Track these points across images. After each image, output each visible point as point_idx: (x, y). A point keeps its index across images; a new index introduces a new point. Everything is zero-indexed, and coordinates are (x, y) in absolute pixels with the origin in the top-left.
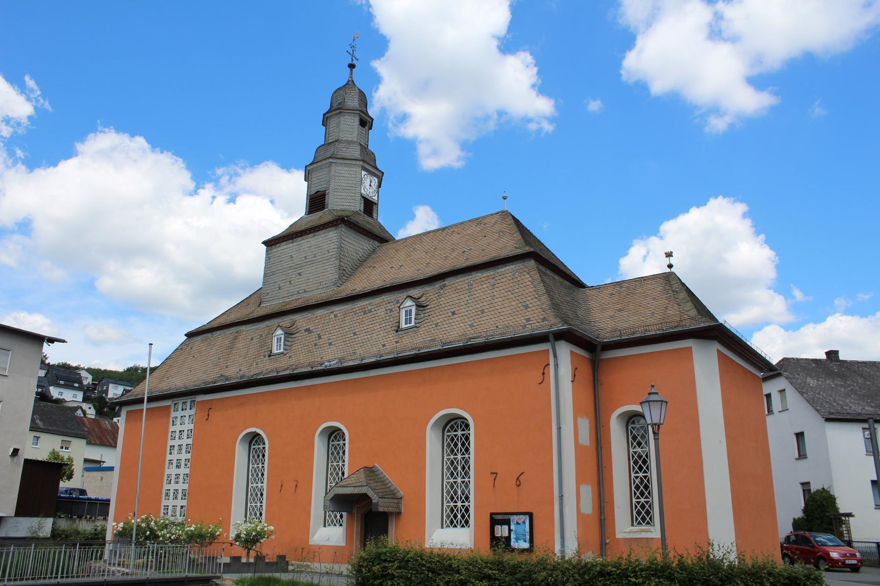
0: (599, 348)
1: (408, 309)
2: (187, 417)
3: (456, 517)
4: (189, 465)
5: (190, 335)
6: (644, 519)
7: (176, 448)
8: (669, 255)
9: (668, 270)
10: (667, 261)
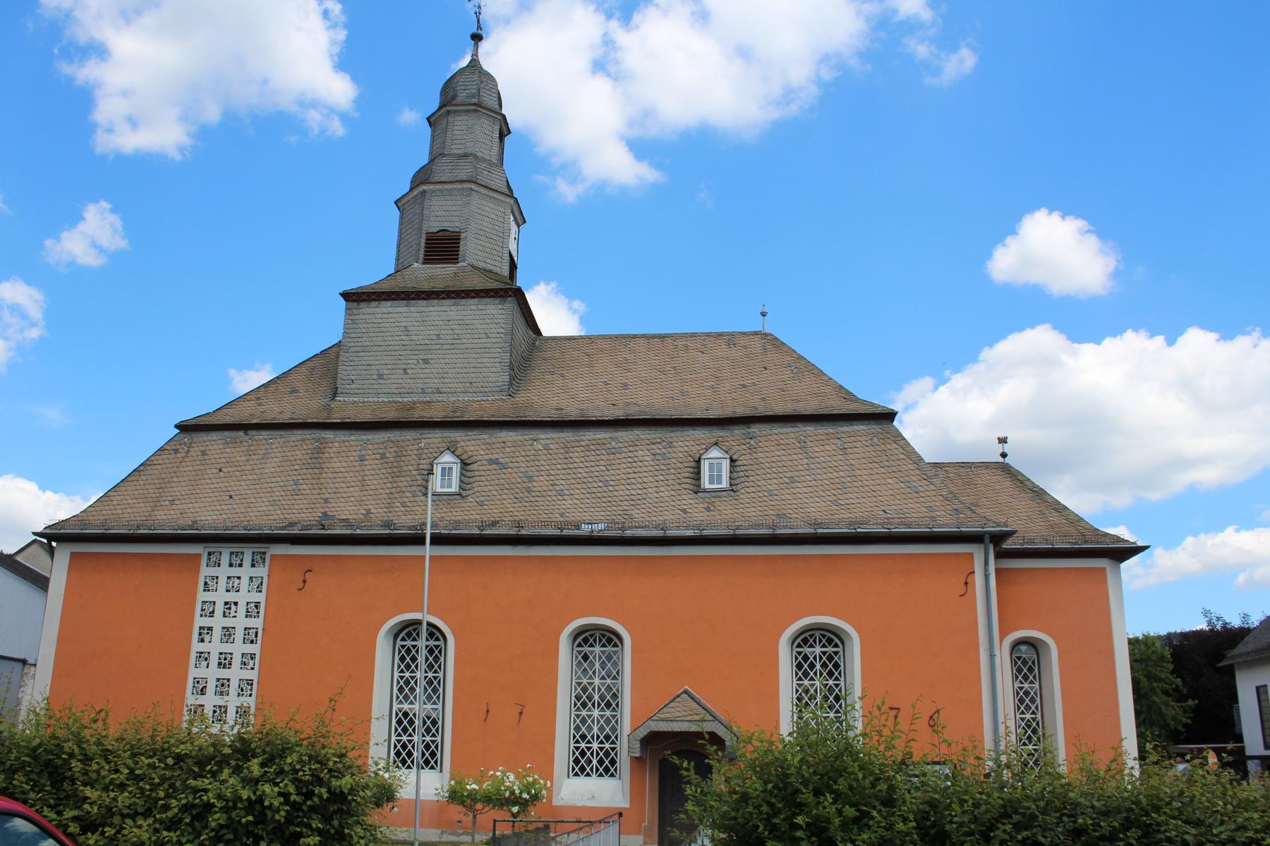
5: (184, 428)
6: (607, 770)
8: (1003, 441)
9: (1001, 460)
10: (1000, 448)
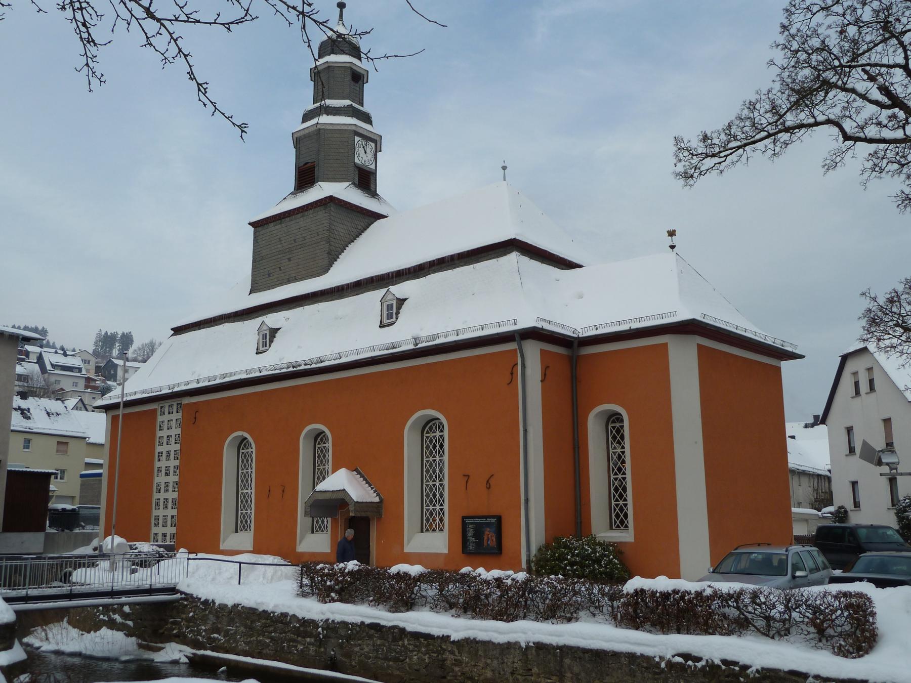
0: (576, 344)
1: (390, 303)
2: (174, 421)
3: (428, 524)
4: (178, 472)
7: (164, 454)
8: (672, 234)
